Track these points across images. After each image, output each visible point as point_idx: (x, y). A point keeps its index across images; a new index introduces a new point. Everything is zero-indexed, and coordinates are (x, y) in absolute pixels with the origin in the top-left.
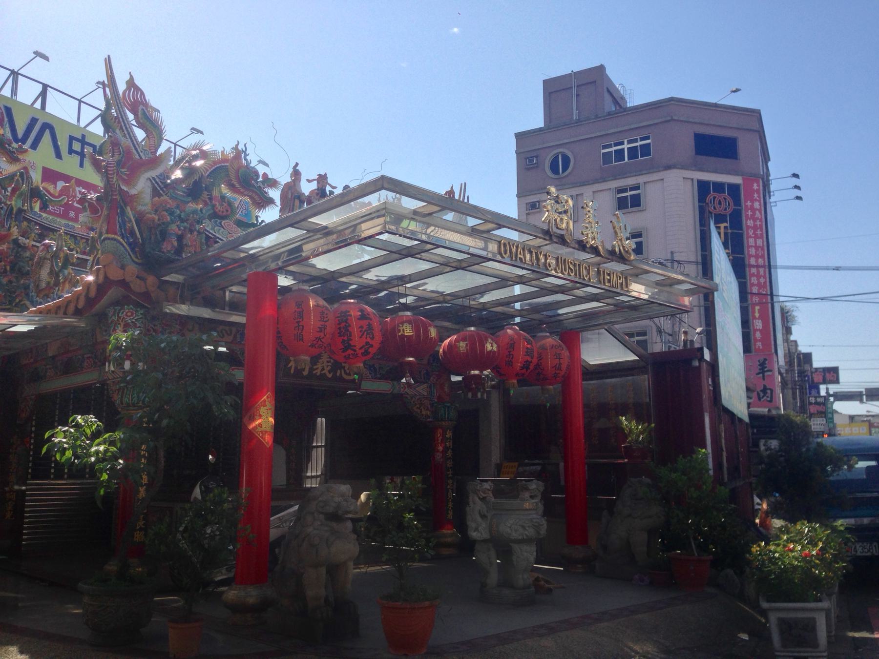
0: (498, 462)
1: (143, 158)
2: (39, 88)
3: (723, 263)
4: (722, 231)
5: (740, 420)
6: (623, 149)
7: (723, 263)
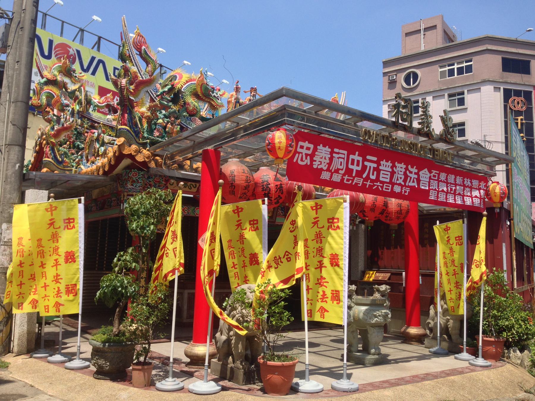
0: (363, 269)
1: (144, 79)
2: (96, 39)
3: (518, 143)
4: (519, 121)
5: (528, 248)
6: (454, 69)
7: (518, 143)
